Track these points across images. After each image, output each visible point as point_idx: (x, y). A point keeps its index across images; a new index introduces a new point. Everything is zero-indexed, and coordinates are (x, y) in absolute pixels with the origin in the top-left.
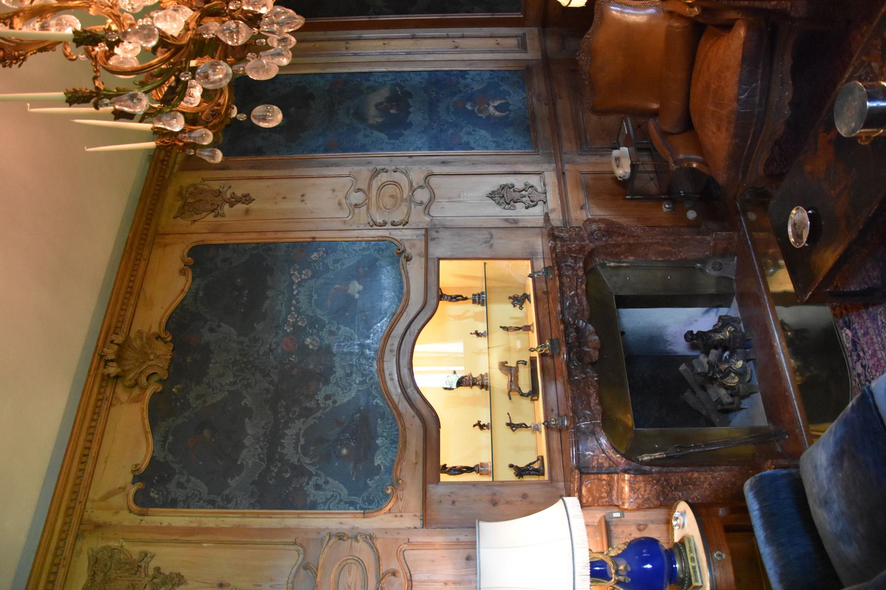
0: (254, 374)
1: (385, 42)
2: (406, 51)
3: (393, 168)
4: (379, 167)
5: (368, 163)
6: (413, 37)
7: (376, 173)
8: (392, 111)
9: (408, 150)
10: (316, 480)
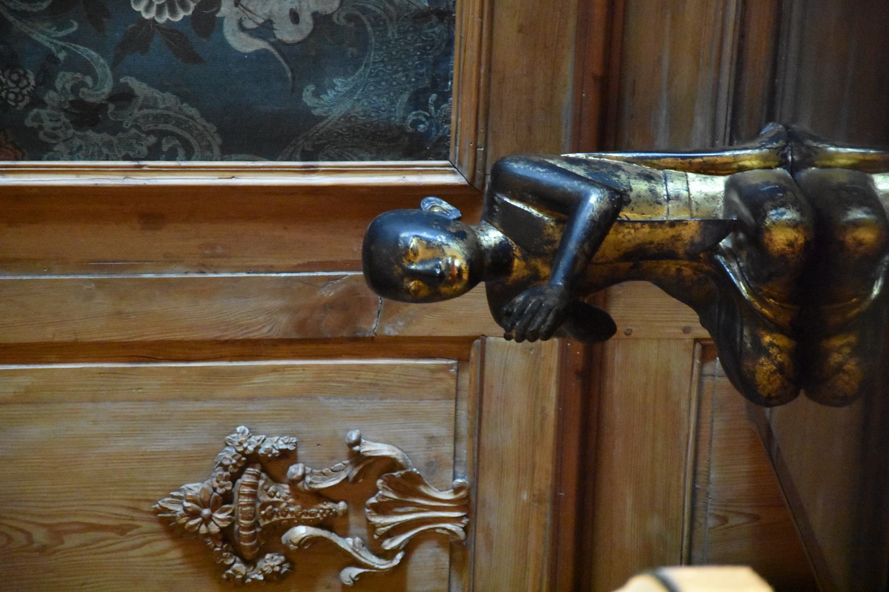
10: (75, 90)
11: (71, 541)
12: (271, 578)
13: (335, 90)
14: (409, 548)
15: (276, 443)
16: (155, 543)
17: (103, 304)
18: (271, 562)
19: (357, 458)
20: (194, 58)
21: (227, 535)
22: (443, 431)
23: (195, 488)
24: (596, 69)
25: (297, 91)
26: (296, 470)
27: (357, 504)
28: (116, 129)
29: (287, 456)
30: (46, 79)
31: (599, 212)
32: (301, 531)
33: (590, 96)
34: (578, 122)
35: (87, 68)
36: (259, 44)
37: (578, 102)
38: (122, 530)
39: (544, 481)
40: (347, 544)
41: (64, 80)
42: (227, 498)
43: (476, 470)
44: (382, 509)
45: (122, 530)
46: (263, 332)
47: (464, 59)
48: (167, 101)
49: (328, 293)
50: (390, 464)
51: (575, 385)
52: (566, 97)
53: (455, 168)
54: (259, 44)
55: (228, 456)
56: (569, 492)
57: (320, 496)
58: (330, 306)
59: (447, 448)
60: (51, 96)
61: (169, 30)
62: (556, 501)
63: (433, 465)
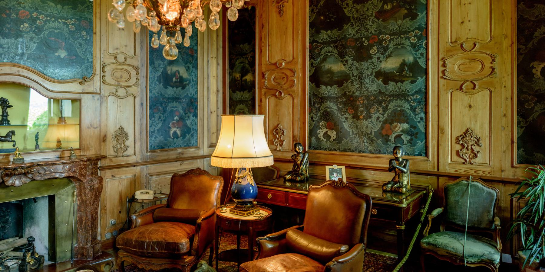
0: (358, 26)
1: (215, 77)
2: (210, 87)
3: (139, 78)
4: (140, 70)
5: (143, 65)
6: (218, 91)
7: (136, 69)
8: (174, 79)
9: (150, 86)
11: (277, 116)
12: (274, 133)
13: (183, 98)
14: (276, 145)
15: (285, 134)
16: (205, 154)
17: (297, 119)
18: (275, 133)
19: (283, 141)
20: (317, 127)
21: (277, 130)
22: (286, 148)
23: (281, 127)
24: (316, 163)
25: (314, 136)
26: (282, 136)
27: (280, 141)
28: (311, 120)
29: (284, 135)
30: (315, 115)
31: (328, 191)
32: (277, 136)
33: (313, 162)
34: (311, 161)
35: (316, 118)
36: (318, 133)
37: (313, 161)
38: (278, 121)
39: (281, 157)
40: (276, 140)
41: (315, 116)
42: (280, 130)
43: (282, 151)
44: (279, 143)
45: (278, 121)
46: (294, 133)
47: (106, 34)
48: (313, 125)
49: (297, 138)
50: (283, 144)
51: (289, 160)
52: (313, 160)
53: (308, 150)
54: (318, 133)
55: (284, 130)
56: (280, 160)
57: (280, 138)
58: (296, 139)
59: (284, 149)
60: (314, 115)
61: (319, 125)
62: (279, 158)
63: (283, 147)
